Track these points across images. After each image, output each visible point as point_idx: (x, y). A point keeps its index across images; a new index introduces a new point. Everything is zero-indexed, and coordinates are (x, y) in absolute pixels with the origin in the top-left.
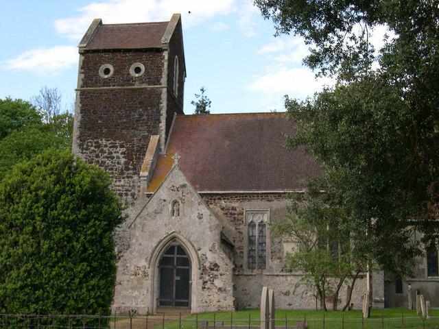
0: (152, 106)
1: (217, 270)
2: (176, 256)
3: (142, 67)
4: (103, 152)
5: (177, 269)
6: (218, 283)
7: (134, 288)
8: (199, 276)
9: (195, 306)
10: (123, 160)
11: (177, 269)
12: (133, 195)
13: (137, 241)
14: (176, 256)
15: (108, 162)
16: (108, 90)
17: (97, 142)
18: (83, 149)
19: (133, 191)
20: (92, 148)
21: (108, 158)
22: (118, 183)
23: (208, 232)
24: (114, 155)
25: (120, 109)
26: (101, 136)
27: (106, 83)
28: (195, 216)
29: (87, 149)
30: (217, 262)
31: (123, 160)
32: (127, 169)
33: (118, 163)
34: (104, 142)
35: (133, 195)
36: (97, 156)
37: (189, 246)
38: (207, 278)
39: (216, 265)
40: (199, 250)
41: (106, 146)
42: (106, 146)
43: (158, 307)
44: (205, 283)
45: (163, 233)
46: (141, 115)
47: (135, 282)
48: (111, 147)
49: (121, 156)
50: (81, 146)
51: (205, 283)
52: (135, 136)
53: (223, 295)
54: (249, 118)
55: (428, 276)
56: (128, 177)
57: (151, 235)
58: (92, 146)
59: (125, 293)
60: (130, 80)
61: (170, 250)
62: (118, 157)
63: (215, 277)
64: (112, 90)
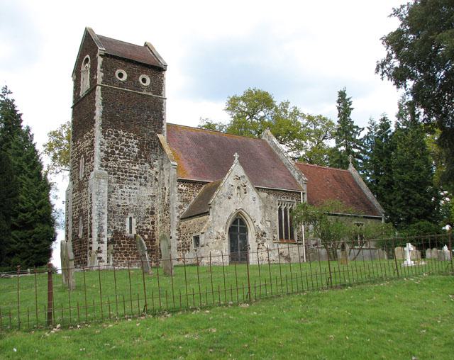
4: (120, 140)
5: (240, 236)
9: (253, 259)
10: (137, 150)
12: (145, 178)
15: (126, 149)
16: (123, 91)
17: (116, 132)
18: (105, 136)
19: (145, 175)
20: (113, 136)
21: (125, 146)
22: (134, 168)
23: (258, 209)
24: (130, 144)
25: (133, 108)
26: (119, 127)
27: (122, 84)
30: (267, 232)
31: (137, 150)
32: (141, 157)
33: (134, 152)
35: (145, 178)
36: (117, 143)
37: (249, 219)
38: (260, 242)
39: (264, 233)
41: (123, 136)
44: (259, 244)
45: (233, 210)
46: (149, 117)
48: (127, 138)
50: (103, 132)
51: (259, 244)
52: (145, 132)
56: (141, 164)
57: (226, 210)
58: (112, 134)
60: (138, 87)
61: (235, 222)
62: (133, 147)
64: (127, 92)
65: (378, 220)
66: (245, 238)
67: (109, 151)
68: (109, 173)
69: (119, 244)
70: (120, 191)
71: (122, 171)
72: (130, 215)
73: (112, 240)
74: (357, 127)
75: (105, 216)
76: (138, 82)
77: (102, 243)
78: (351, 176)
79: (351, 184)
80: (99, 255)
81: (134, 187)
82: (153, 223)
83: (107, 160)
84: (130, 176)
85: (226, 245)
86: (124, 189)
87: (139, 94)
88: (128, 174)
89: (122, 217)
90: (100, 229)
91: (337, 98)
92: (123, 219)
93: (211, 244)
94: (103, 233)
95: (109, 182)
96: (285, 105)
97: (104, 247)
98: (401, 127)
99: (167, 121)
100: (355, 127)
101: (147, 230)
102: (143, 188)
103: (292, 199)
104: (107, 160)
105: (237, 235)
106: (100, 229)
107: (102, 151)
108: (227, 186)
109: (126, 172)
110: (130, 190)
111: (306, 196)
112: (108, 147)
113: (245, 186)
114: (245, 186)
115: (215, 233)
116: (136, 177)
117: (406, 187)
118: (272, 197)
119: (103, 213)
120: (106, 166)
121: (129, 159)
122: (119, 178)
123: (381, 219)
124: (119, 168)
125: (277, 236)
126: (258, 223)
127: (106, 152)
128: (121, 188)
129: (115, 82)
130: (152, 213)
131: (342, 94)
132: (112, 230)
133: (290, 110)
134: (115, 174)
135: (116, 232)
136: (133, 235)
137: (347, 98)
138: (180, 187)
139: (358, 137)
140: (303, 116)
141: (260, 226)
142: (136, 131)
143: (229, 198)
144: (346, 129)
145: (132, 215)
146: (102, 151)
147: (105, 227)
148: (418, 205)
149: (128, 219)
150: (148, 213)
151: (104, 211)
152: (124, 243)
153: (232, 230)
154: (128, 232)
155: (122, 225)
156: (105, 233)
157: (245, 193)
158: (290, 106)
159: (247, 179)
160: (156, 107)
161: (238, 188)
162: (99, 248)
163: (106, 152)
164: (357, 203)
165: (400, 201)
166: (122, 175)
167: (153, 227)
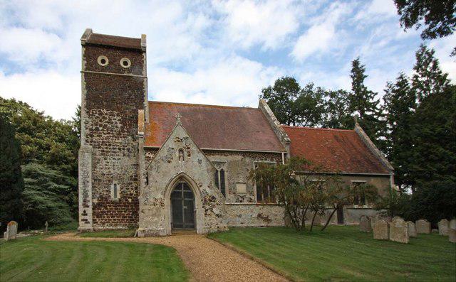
0: (138, 89)
1: (214, 201)
2: (183, 191)
3: (122, 63)
4: (104, 118)
5: (185, 201)
6: (216, 211)
7: (154, 215)
8: (202, 205)
10: (119, 125)
11: (185, 201)
12: (128, 150)
13: (154, 178)
14: (183, 191)
18: (90, 115)
21: (108, 123)
23: (206, 173)
24: (113, 121)
26: (103, 108)
27: (104, 69)
28: (196, 161)
29: (92, 115)
30: (217, 197)
31: (119, 125)
32: (124, 132)
34: (105, 111)
36: (101, 121)
37: (194, 183)
38: (208, 207)
39: (213, 198)
40: (201, 186)
41: (106, 114)
42: (106, 114)
43: (172, 229)
44: (206, 210)
45: (173, 174)
46: (130, 95)
47: (154, 210)
49: (118, 122)
50: (88, 112)
51: (206, 210)
53: (220, 219)
54: (186, 108)
55: (18, 232)
59: (147, 219)
60: (120, 69)
61: (178, 186)
63: (214, 206)
64: (108, 75)
65: (385, 178)
66: (191, 205)
67: (94, 128)
68: (94, 148)
69: (106, 207)
70: (104, 162)
71: (106, 145)
72: (114, 182)
73: (99, 204)
74: (371, 92)
75: (90, 185)
76: (119, 65)
77: (88, 207)
78: (357, 134)
79: (355, 143)
80: (85, 217)
81: (116, 158)
82: (136, 188)
83: (92, 136)
84: (113, 149)
85: (167, 211)
86: (108, 161)
87: (120, 76)
88: (111, 147)
89: (106, 184)
90: (86, 195)
91: (351, 68)
92: (108, 185)
93: (147, 211)
94: (88, 199)
95: (94, 154)
96: (310, 87)
97: (90, 211)
98: (420, 79)
99: (149, 99)
100: (368, 92)
101: (131, 194)
102: (126, 158)
103: (272, 160)
104: (92, 136)
105: (181, 201)
106: (86, 195)
107: (87, 129)
108: (166, 150)
109: (110, 145)
110: (114, 161)
111: (288, 156)
112: (92, 125)
113: (189, 148)
114: (189, 148)
115: (152, 200)
116: (119, 149)
117: (425, 142)
118: (247, 160)
119: (88, 182)
120: (91, 142)
121: (112, 134)
122: (103, 151)
123: (389, 177)
124: (103, 142)
125: (255, 198)
126: (205, 187)
127: (91, 130)
128: (105, 159)
129: (97, 67)
130: (136, 180)
131: (356, 63)
132: (98, 195)
133: (315, 90)
134: (100, 147)
135: (102, 197)
136: (117, 200)
137: (359, 66)
138: (147, 155)
139: (371, 101)
140: (327, 94)
141: (208, 190)
142: (119, 109)
143: (169, 162)
144: (360, 98)
145: (116, 182)
146: (87, 129)
147: (90, 193)
148: (441, 160)
149: (112, 186)
150: (131, 179)
151: (88, 179)
152: (110, 206)
153: (174, 196)
154: (113, 197)
155: (107, 191)
156: (89, 198)
157: (189, 155)
158: (314, 87)
159: (190, 141)
160: (137, 88)
161: (181, 150)
162: (85, 211)
163: (90, 129)
164: (359, 162)
165: (418, 157)
166: (107, 148)
167: (137, 192)
